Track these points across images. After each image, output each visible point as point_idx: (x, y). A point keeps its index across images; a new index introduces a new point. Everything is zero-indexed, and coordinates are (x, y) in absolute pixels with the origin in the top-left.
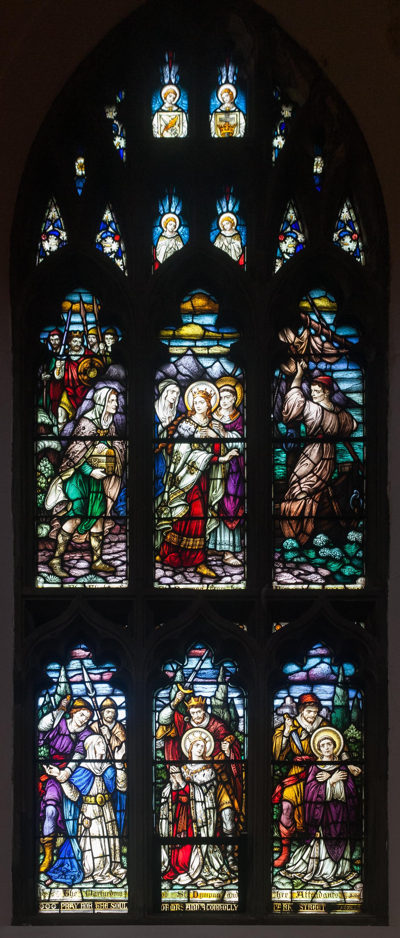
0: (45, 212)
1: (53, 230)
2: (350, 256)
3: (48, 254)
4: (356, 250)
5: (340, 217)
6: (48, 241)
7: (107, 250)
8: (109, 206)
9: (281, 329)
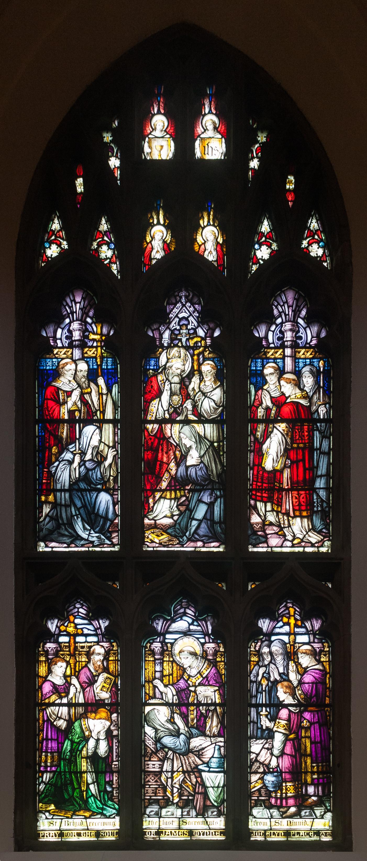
0: (49, 224)
1: (265, 241)
2: (317, 261)
3: (50, 259)
4: (322, 255)
5: (99, 228)
6: (50, 249)
7: (103, 256)
8: (316, 216)
9: (256, 325)
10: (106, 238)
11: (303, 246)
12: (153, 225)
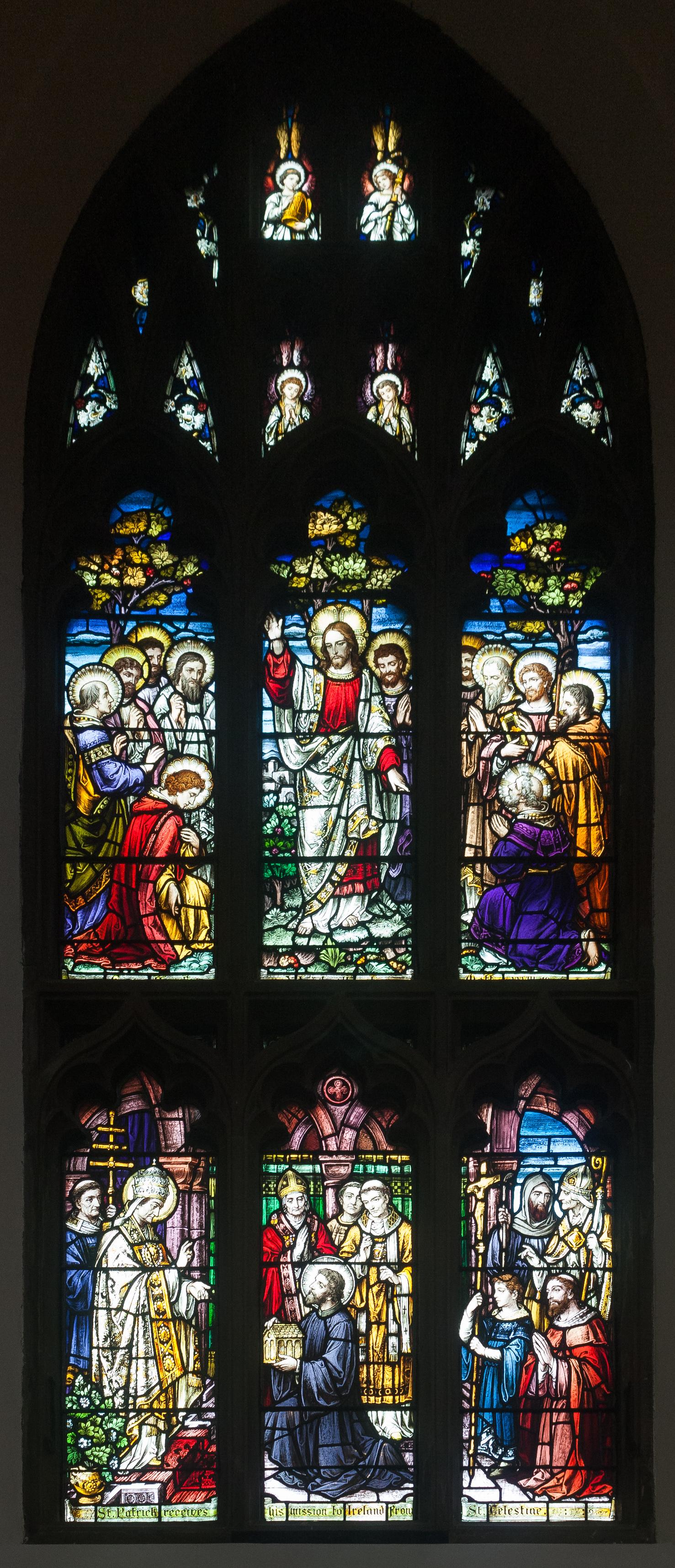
1: (489, 398)
7: (492, 428)
10: (189, 392)
11: (167, 411)
12: (281, 369)
